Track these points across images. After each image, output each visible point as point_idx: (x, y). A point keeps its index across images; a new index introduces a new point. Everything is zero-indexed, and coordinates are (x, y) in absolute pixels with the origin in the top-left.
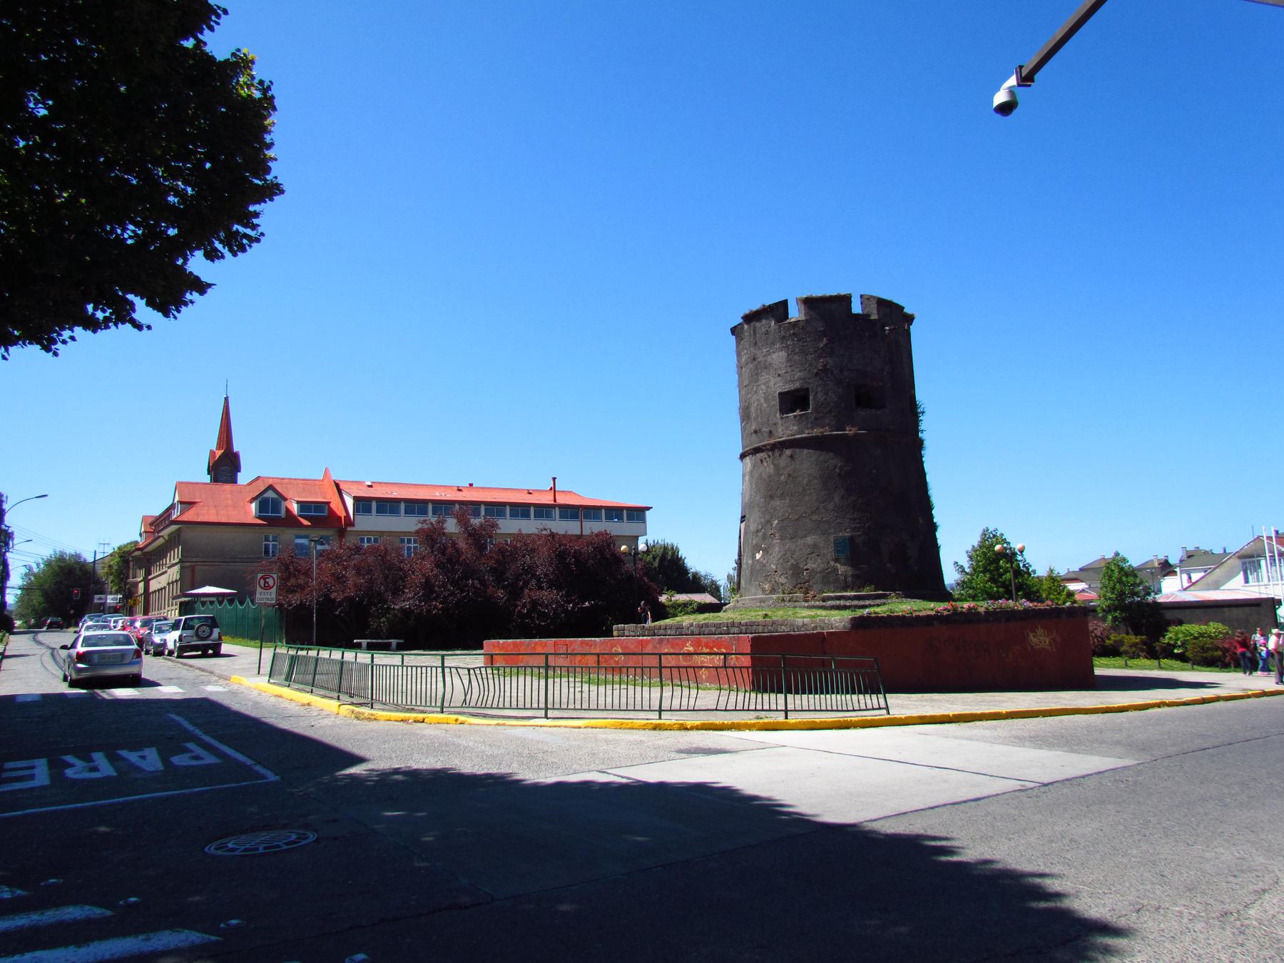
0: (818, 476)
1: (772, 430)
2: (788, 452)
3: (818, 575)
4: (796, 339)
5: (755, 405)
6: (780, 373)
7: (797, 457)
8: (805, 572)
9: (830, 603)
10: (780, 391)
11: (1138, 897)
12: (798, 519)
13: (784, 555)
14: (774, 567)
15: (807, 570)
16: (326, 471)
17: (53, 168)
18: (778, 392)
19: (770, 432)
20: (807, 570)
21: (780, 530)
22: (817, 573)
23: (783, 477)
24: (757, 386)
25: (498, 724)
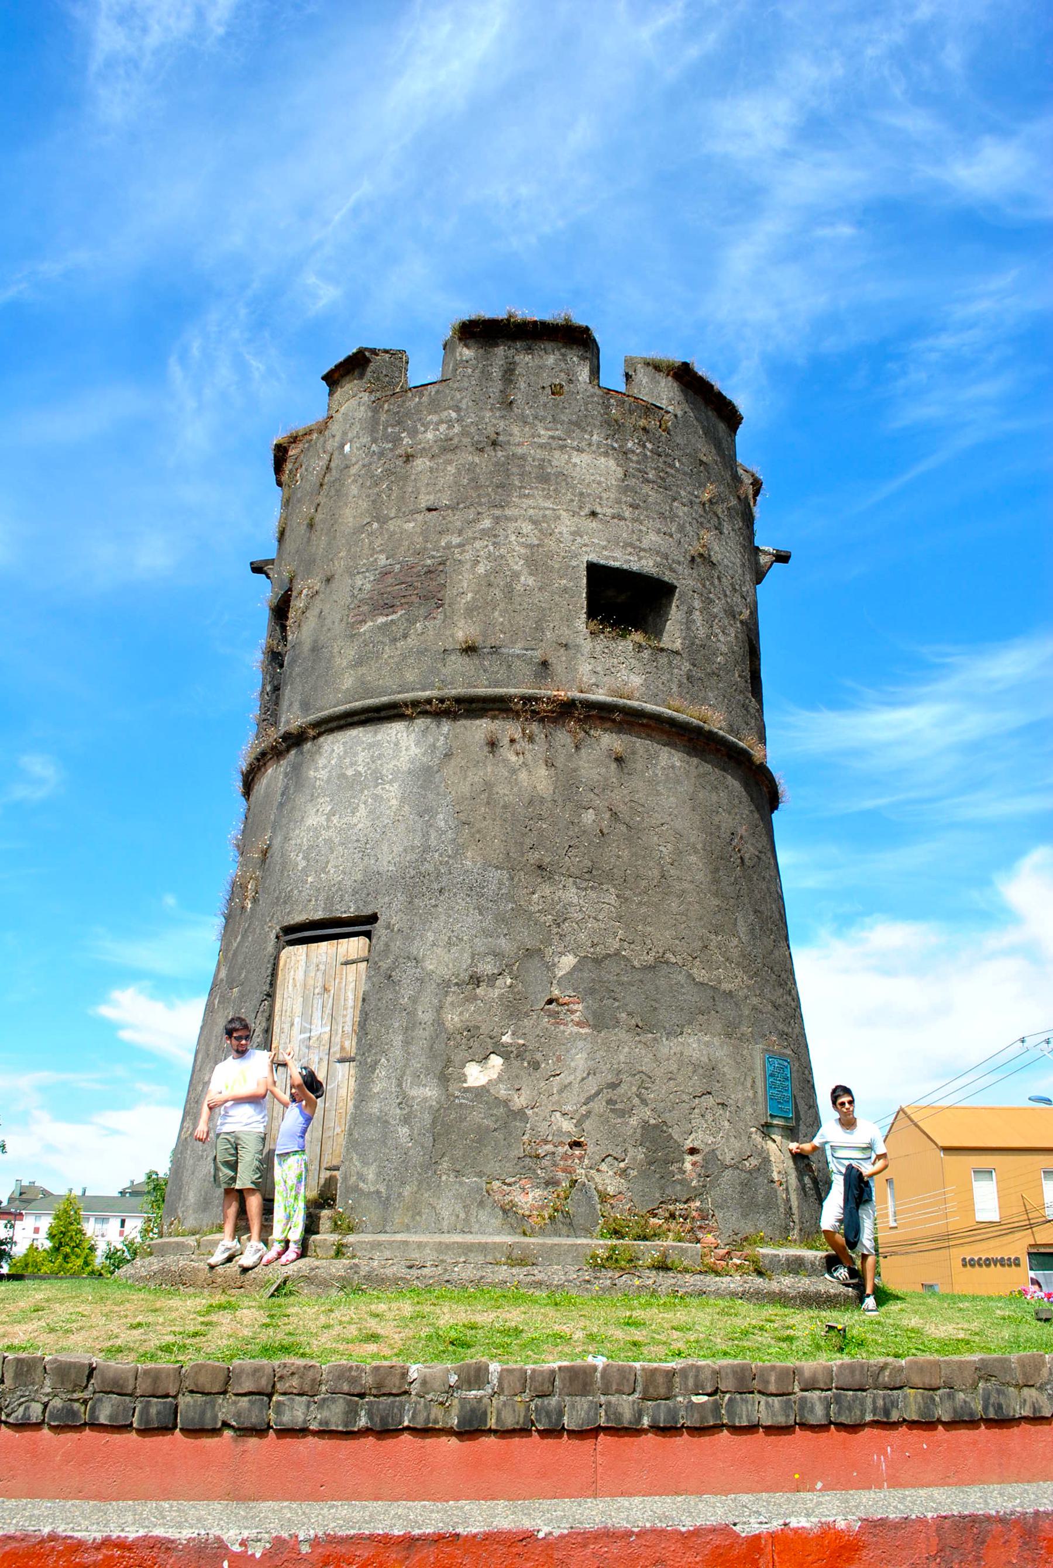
0: (699, 846)
1: (552, 660)
2: (609, 741)
3: (728, 1173)
4: (649, 446)
5: (481, 569)
6: (598, 510)
7: (639, 766)
8: (689, 1158)
9: (786, 1283)
10: (593, 558)
11: (761, 1523)
12: (651, 968)
13: (614, 1086)
14: (567, 1126)
15: (693, 1151)
16: (71, 1190)
17: (855, 1474)
18: (585, 559)
19: (545, 664)
20: (693, 1151)
21: (592, 991)
22: (727, 1167)
23: (589, 817)
24: (497, 520)
25: (475, 687)
